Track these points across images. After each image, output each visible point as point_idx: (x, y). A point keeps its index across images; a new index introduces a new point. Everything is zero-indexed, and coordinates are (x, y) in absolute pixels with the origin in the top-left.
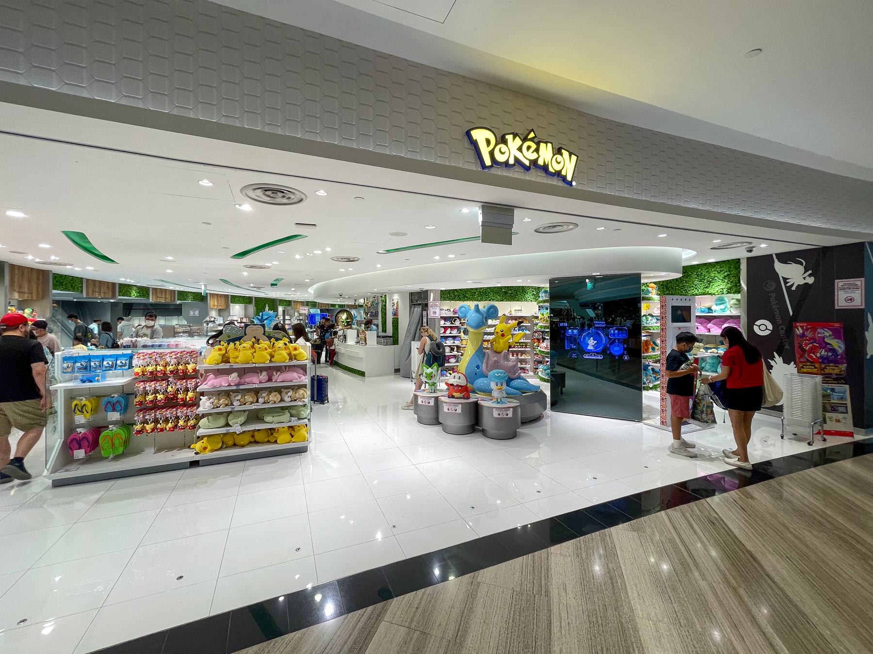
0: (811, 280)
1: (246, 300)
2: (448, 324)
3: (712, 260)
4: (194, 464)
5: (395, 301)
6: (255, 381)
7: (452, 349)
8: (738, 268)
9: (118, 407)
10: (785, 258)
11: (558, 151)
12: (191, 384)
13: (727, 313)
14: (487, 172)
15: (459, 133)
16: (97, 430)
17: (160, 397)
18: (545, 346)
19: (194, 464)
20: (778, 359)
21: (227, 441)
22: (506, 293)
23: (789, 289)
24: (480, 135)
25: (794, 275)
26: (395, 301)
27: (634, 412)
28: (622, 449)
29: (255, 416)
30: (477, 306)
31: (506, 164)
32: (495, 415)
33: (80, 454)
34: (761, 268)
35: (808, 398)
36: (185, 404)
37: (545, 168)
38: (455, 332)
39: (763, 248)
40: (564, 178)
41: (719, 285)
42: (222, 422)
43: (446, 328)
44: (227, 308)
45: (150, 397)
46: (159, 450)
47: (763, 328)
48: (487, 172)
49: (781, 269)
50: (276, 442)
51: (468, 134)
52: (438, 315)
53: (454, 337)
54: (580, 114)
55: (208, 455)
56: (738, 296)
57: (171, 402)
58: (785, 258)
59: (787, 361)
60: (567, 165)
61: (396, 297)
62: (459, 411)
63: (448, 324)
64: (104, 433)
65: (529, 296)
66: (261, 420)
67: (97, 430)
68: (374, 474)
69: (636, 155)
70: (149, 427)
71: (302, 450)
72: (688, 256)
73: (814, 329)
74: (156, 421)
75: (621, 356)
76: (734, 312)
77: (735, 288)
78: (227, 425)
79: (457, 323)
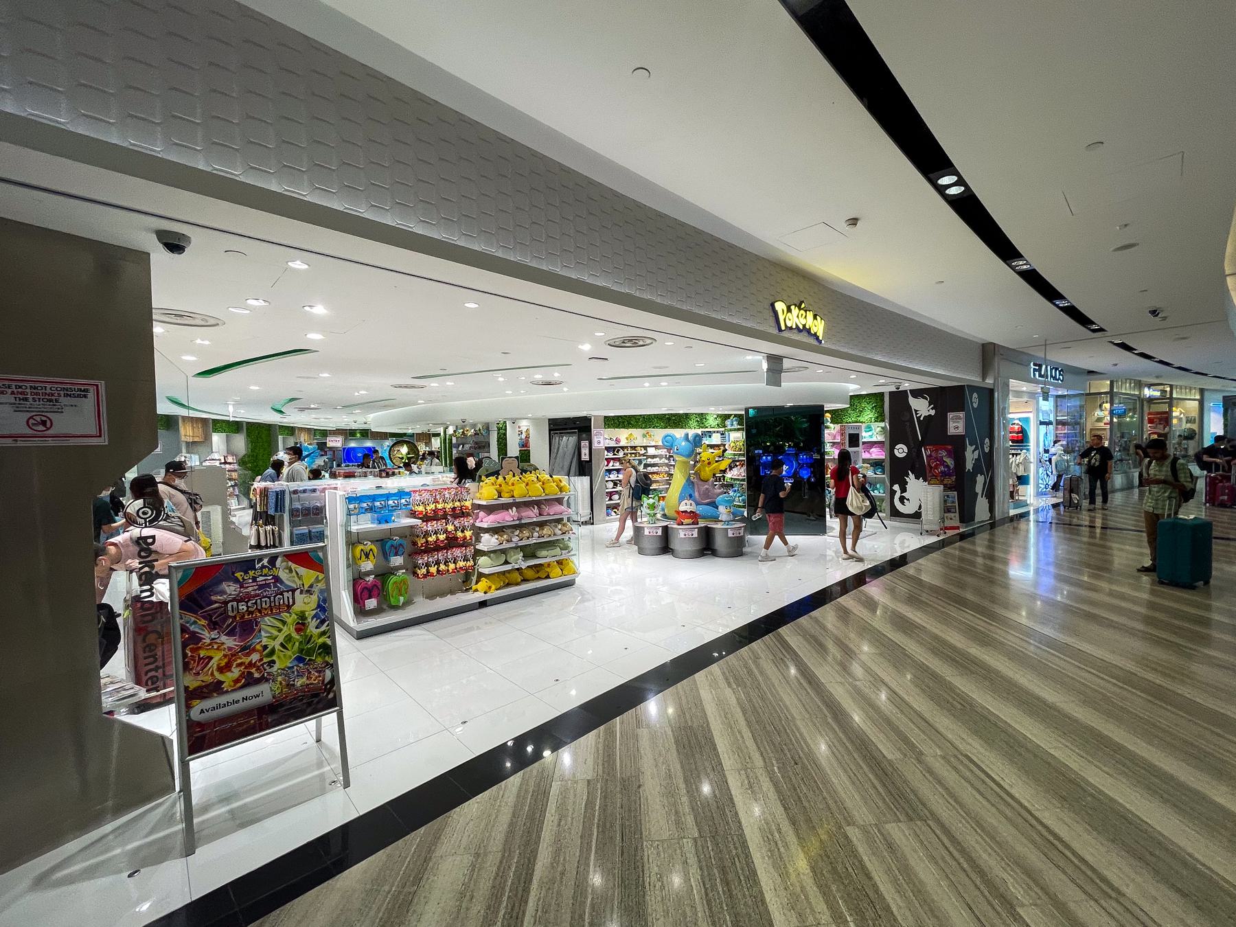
0: (933, 412)
1: (234, 427)
2: (611, 455)
3: (864, 393)
4: (483, 604)
5: (524, 429)
6: (531, 515)
7: (615, 484)
8: (883, 400)
9: (371, 556)
10: (917, 393)
11: (815, 317)
12: (467, 522)
13: (874, 439)
14: (779, 333)
15: (768, 306)
16: (384, 574)
17: (442, 537)
18: (739, 473)
19: (483, 604)
20: (912, 476)
21: (505, 579)
22: (669, 419)
23: (918, 418)
24: (780, 306)
25: (922, 408)
26: (524, 429)
27: (821, 529)
28: (811, 560)
29: (529, 552)
30: (687, 435)
31: (791, 328)
32: (730, 535)
33: (371, 603)
34: (899, 398)
35: (937, 500)
36: (465, 544)
37: (809, 331)
38: (617, 465)
39: (906, 386)
40: (817, 338)
41: (868, 415)
42: (503, 559)
43: (608, 460)
44: (207, 439)
45: (432, 539)
46: (431, 596)
47: (901, 451)
48: (779, 333)
49: (915, 403)
50: (548, 577)
51: (773, 305)
52: (602, 446)
53: (618, 471)
54: (825, 287)
55: (494, 594)
56: (882, 424)
57: (452, 542)
58: (917, 393)
59: (917, 478)
60: (818, 327)
61: (524, 425)
62: (696, 535)
63: (611, 455)
64: (393, 579)
65: (693, 423)
66: (534, 556)
67: (384, 574)
68: (635, 600)
69: (862, 321)
70: (433, 570)
71: (569, 584)
72: (853, 388)
73: (937, 451)
74: (438, 563)
75: (809, 479)
76: (880, 438)
77: (880, 418)
78: (506, 562)
79: (621, 454)
